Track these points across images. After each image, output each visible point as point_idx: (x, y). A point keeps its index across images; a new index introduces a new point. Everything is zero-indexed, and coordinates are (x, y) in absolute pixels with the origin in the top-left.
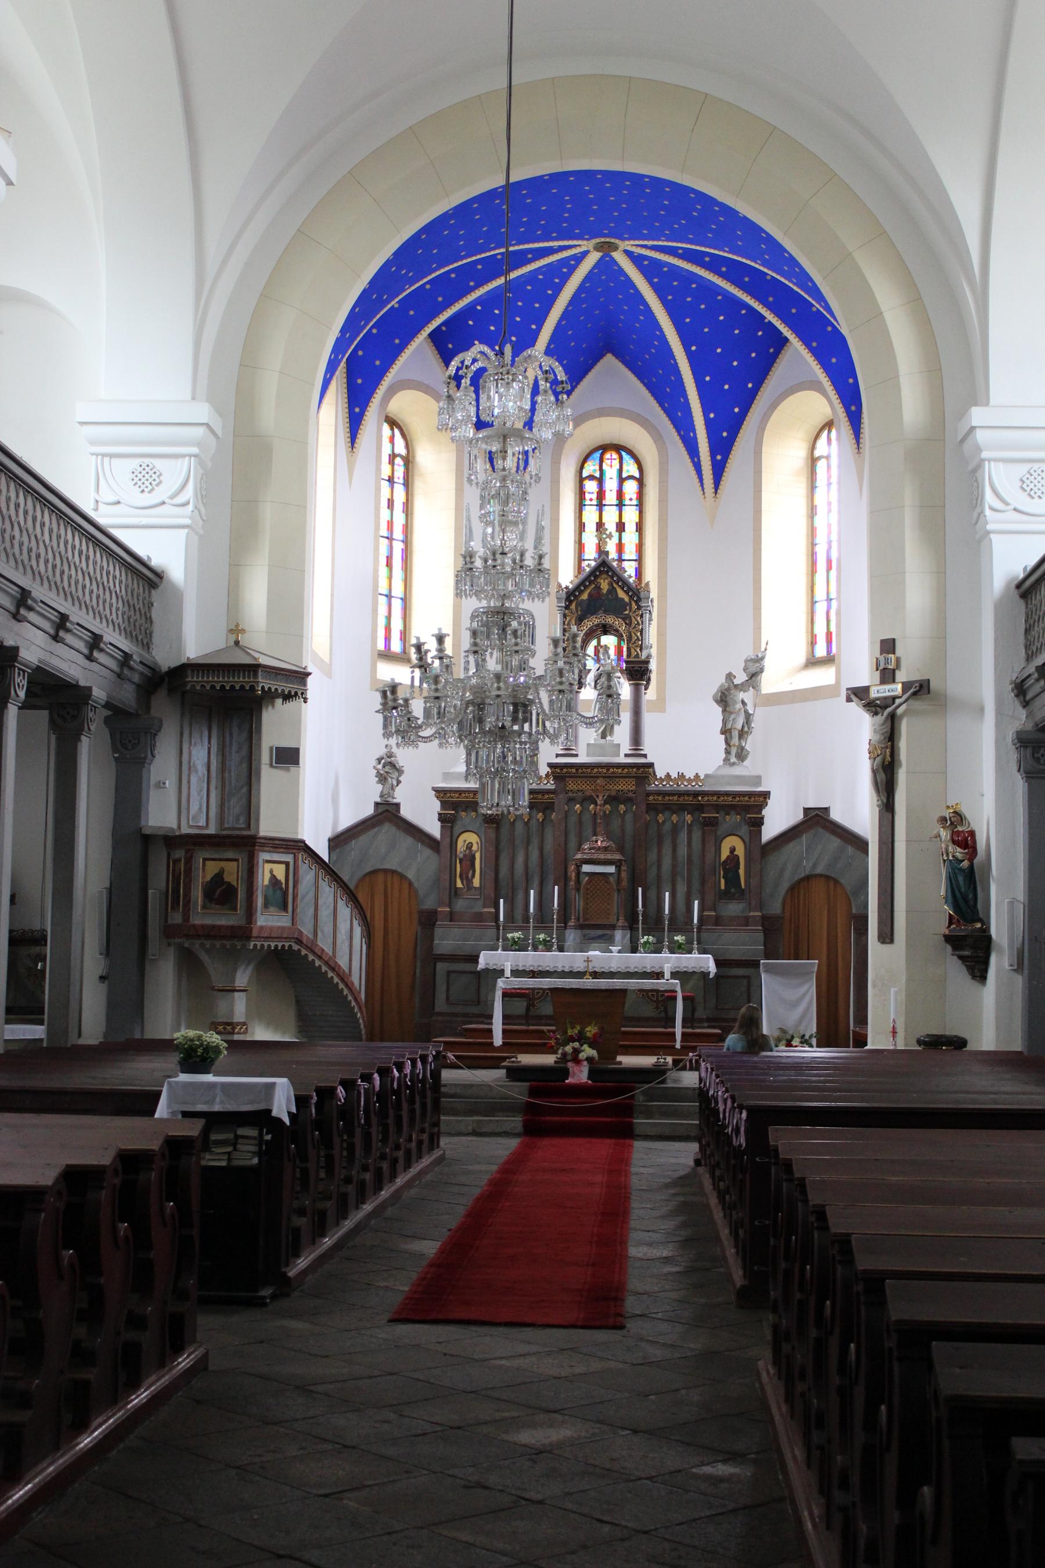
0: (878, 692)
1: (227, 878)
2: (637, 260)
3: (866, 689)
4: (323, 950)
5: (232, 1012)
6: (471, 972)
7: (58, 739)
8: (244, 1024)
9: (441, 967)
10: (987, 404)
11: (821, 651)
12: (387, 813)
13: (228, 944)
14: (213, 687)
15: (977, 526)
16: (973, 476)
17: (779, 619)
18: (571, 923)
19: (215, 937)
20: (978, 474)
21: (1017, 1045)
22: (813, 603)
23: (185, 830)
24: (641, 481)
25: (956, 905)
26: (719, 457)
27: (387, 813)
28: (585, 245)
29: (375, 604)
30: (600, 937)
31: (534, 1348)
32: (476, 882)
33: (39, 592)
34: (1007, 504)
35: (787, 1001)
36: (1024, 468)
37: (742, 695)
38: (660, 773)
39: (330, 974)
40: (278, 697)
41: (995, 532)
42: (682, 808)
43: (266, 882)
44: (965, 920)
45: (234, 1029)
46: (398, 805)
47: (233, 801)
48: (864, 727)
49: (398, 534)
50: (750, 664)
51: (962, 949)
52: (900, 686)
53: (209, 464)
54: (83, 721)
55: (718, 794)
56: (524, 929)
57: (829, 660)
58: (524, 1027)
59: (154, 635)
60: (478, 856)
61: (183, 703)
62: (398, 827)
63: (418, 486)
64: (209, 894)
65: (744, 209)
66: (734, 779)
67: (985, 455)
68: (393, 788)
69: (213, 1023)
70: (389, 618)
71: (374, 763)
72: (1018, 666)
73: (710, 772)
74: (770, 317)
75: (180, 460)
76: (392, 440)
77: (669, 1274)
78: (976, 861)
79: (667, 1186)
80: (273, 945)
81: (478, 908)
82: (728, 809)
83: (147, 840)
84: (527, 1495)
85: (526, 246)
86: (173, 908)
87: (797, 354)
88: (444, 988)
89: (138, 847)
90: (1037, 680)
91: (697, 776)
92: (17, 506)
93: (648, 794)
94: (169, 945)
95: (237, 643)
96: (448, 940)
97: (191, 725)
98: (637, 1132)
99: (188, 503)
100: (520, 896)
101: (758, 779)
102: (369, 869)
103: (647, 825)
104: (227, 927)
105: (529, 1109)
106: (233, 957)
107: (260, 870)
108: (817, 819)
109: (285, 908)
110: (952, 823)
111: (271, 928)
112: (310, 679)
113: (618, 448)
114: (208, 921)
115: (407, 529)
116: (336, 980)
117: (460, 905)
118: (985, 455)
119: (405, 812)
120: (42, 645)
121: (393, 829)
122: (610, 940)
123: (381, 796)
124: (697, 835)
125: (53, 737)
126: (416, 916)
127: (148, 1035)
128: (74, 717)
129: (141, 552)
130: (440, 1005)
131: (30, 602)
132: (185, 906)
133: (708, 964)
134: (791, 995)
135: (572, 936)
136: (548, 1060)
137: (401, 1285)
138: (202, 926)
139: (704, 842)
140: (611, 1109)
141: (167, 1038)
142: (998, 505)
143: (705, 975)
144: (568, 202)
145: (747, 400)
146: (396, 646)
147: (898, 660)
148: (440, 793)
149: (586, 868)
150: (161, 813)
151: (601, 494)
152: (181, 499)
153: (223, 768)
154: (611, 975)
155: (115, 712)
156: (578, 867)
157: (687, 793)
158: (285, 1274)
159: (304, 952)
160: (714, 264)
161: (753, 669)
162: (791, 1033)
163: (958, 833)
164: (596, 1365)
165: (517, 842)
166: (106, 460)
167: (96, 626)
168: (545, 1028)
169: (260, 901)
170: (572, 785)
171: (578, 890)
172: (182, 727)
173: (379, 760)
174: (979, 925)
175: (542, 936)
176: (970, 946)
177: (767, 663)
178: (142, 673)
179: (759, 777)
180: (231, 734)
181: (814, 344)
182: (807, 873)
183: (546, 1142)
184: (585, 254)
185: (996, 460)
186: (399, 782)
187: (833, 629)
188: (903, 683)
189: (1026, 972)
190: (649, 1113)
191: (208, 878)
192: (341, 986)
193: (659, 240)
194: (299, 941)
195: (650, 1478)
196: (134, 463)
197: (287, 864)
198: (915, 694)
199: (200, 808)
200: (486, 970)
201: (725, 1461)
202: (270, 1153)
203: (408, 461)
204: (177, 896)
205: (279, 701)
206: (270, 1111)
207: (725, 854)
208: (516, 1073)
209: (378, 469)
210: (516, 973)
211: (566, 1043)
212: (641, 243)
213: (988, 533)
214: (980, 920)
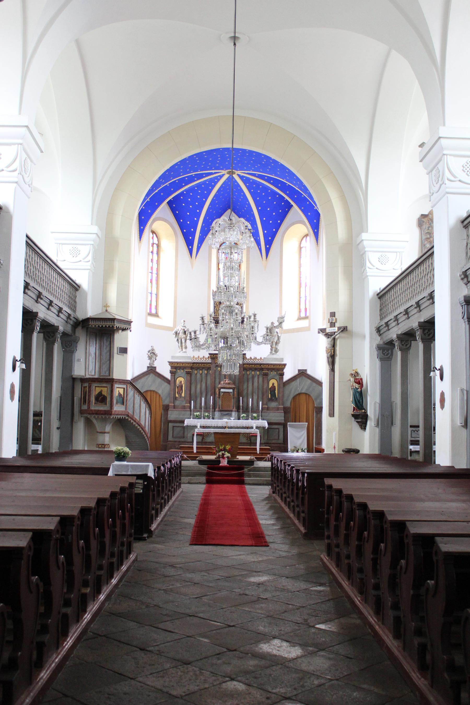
0: (329, 330)
1: (103, 393)
2: (241, 177)
3: (325, 329)
5: (104, 439)
6: (181, 427)
7: (47, 344)
8: (108, 445)
10: (367, 232)
11: (303, 315)
12: (152, 370)
13: (104, 416)
14: (99, 326)
15: (364, 274)
16: (362, 256)
17: (297, 305)
18: (217, 409)
19: (99, 414)
21: (377, 452)
22: (300, 298)
23: (88, 376)
25: (356, 404)
26: (268, 246)
27: (152, 370)
28: (223, 172)
30: (227, 414)
31: (242, 553)
33: (45, 293)
34: (374, 266)
35: (297, 436)
36: (379, 254)
37: (277, 330)
40: (120, 329)
41: (370, 276)
42: (256, 369)
43: (117, 395)
45: (105, 446)
46: (155, 367)
47: (104, 366)
49: (155, 271)
50: (279, 319)
51: (358, 419)
52: (336, 329)
55: (268, 364)
56: (200, 411)
57: (306, 318)
60: (184, 386)
61: (87, 332)
62: (156, 375)
63: (162, 254)
64: (97, 399)
65: (273, 157)
66: (274, 359)
67: (366, 249)
69: (97, 444)
70: (151, 301)
71: (147, 352)
72: (377, 322)
73: (266, 357)
74: (287, 198)
75: (13, 146)
76: (153, 238)
77: (275, 529)
78: (363, 389)
79: (263, 500)
80: (119, 417)
81: (184, 404)
82: (272, 370)
83: (74, 379)
84: (261, 597)
85: (204, 172)
86: (83, 404)
87: (296, 211)
88: (172, 432)
89: (71, 382)
90: (385, 327)
91: (261, 358)
92: (37, 263)
95: (107, 311)
96: (173, 415)
98: (246, 482)
99: (89, 261)
101: (282, 359)
103: (244, 375)
105: (208, 475)
106: (105, 421)
108: (302, 373)
109: (123, 404)
111: (119, 411)
112: (132, 324)
115: (158, 270)
116: (140, 429)
117: (177, 403)
118: (366, 249)
119: (158, 370)
120: (44, 311)
122: (230, 415)
123: (150, 364)
124: (261, 379)
125: (45, 344)
126: (162, 407)
127: (74, 448)
128: (53, 337)
129: (74, 278)
130: (170, 438)
131: (42, 296)
132: (88, 404)
133: (265, 424)
134: (298, 435)
135: (217, 414)
136: (213, 457)
137: (188, 534)
138: (95, 410)
140: (236, 474)
141: (81, 449)
143: (264, 428)
144: (219, 157)
145: (278, 227)
146: (154, 311)
147: (336, 319)
148: (170, 363)
149: (222, 390)
150: (79, 370)
152: (12, 168)
153: (100, 354)
155: (64, 334)
156: (219, 390)
157: (258, 364)
158: (151, 529)
160: (269, 180)
161: (281, 321)
162: (298, 448)
163: (357, 379)
164: (265, 558)
165: (198, 381)
167: (61, 305)
168: (212, 446)
169: (115, 401)
171: (219, 398)
172: (86, 340)
173: (149, 352)
174: (364, 411)
175: (207, 414)
176: (361, 418)
177: (285, 319)
178: (73, 321)
181: (303, 208)
183: (215, 486)
184: (223, 175)
185: (370, 251)
186: (156, 359)
187: (307, 307)
189: (380, 427)
190: (249, 476)
191: (97, 393)
192: (142, 431)
193: (250, 171)
194: (128, 416)
195: (298, 591)
196: (70, 247)
197: (124, 389)
198: (342, 331)
200: (187, 426)
201: (320, 586)
202: (145, 488)
203: (158, 246)
204: (85, 399)
205: (121, 331)
206: (147, 474)
207: (271, 385)
208: (202, 462)
209: (149, 248)
210: (201, 427)
211: (219, 452)
212: (244, 172)
213: (367, 276)
214: (364, 409)
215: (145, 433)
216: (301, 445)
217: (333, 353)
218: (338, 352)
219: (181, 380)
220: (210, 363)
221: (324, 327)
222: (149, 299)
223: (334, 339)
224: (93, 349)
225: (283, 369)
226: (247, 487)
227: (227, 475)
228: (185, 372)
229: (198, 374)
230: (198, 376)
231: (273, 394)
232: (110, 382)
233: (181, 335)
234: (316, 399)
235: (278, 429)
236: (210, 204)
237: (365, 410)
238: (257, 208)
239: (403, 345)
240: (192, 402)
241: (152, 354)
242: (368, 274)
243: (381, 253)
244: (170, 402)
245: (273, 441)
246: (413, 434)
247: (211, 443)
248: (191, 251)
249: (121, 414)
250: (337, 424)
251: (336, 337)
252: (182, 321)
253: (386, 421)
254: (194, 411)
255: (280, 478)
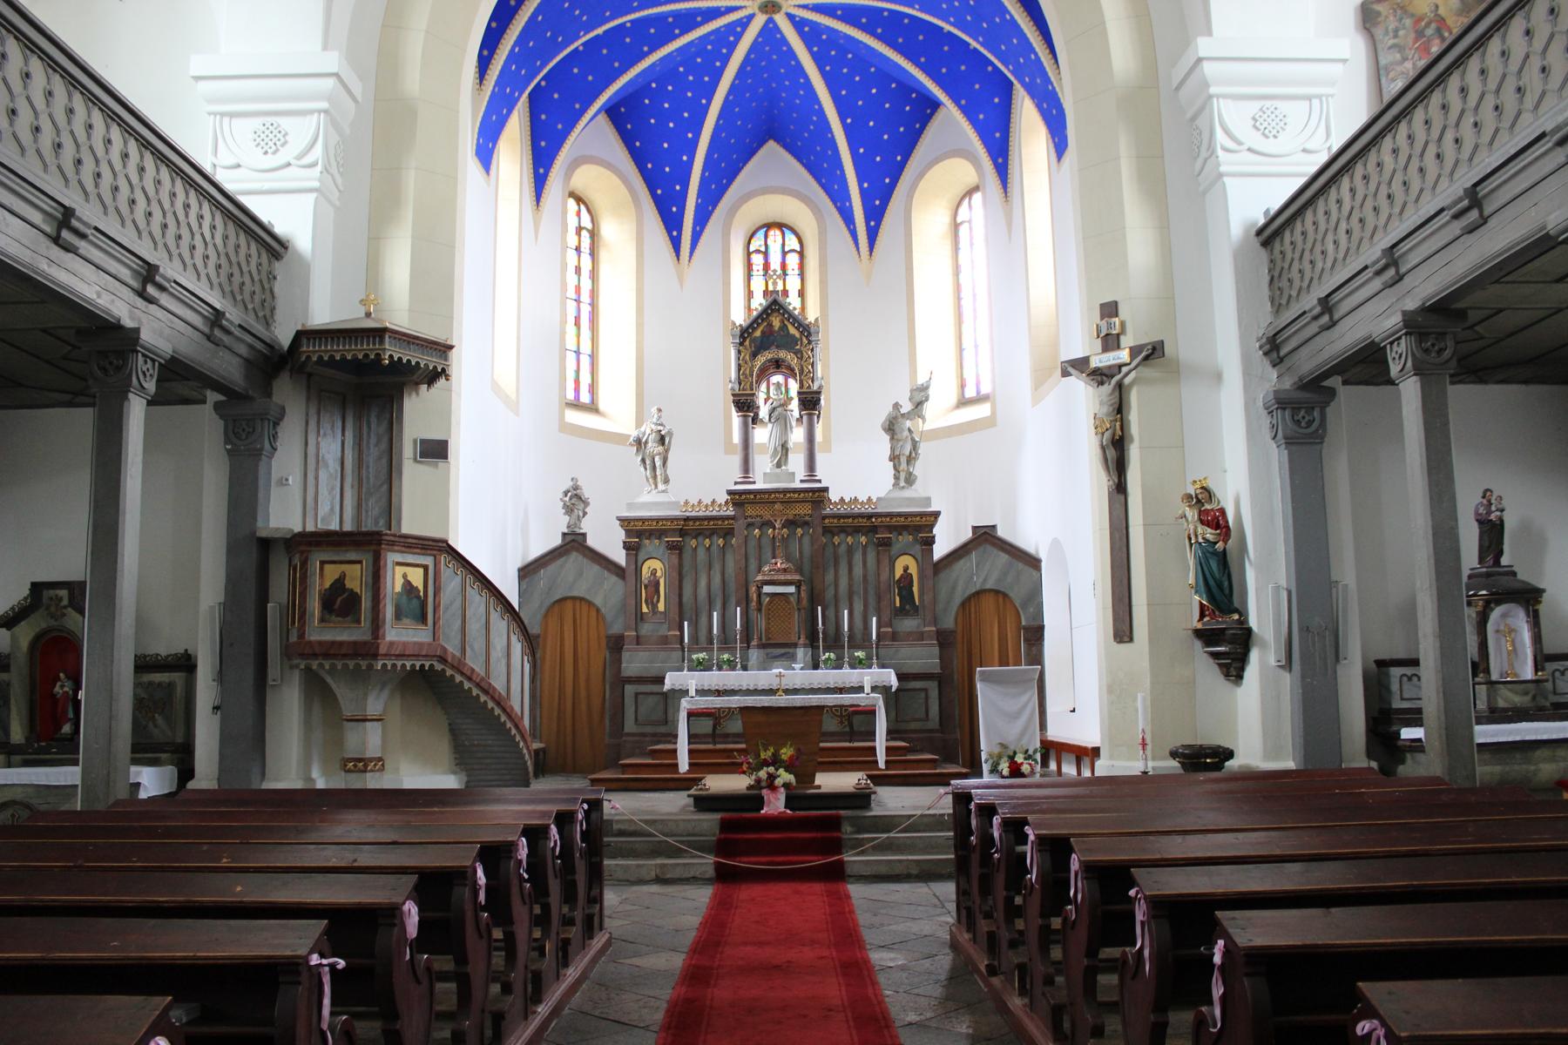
0: (1100, 360)
1: (349, 584)
3: (1086, 360)
4: (473, 670)
8: (380, 759)
9: (630, 689)
12: (574, 542)
13: (351, 664)
18: (754, 643)
19: (335, 656)
20: (1201, 122)
22: (961, 350)
24: (801, 254)
27: (574, 542)
29: (563, 359)
30: (782, 655)
32: (661, 607)
34: (1240, 143)
37: (908, 423)
38: (834, 496)
39: (483, 698)
42: (857, 530)
43: (398, 588)
44: (1221, 611)
45: (366, 766)
46: (584, 535)
47: (372, 501)
48: (1083, 401)
49: (585, 297)
52: (1124, 355)
53: (348, 131)
54: (130, 375)
55: (891, 515)
56: (709, 650)
58: (710, 746)
59: (277, 311)
60: (662, 582)
61: (309, 387)
63: (603, 255)
64: (328, 603)
66: (905, 502)
67: (1213, 90)
68: (579, 519)
71: (561, 495)
72: (1264, 320)
73: (882, 495)
75: (308, 118)
81: (663, 630)
82: (900, 529)
83: (266, 545)
89: (260, 557)
91: (869, 499)
93: (824, 518)
94: (292, 667)
96: (634, 663)
97: (319, 414)
98: (849, 871)
99: (314, 164)
100: (703, 620)
102: (557, 597)
103: (824, 547)
104: (349, 643)
105: (722, 847)
106: (362, 678)
107: (389, 574)
108: (985, 537)
110: (1199, 501)
111: (405, 644)
112: (454, 354)
113: (781, 226)
114: (328, 636)
115: (594, 294)
116: (491, 704)
117: (646, 629)
118: (1213, 90)
119: (591, 542)
121: (580, 557)
122: (793, 658)
124: (871, 556)
128: (118, 369)
129: (264, 218)
130: (630, 726)
134: (1011, 705)
135: (754, 655)
138: (321, 643)
139: (878, 561)
142: (1230, 144)
145: (897, 171)
146: (585, 398)
147: (1123, 324)
148: (624, 522)
149: (767, 589)
150: (284, 514)
151: (766, 266)
152: (308, 159)
153: (360, 463)
154: (795, 691)
156: (759, 588)
159: (449, 672)
161: (918, 398)
162: (1012, 748)
163: (1207, 511)
166: (226, 120)
169: (389, 611)
170: (750, 511)
171: (759, 610)
173: (566, 494)
174: (1236, 617)
175: (726, 656)
176: (1227, 643)
177: (931, 392)
178: (251, 346)
179: (929, 499)
180: (369, 427)
182: (978, 587)
184: (751, 17)
185: (1225, 96)
186: (585, 514)
188: (1131, 349)
191: (327, 585)
192: (497, 711)
194: (443, 660)
196: (256, 123)
197: (426, 568)
198: (1147, 358)
199: (332, 509)
200: (673, 691)
203: (593, 234)
204: (296, 612)
207: (899, 573)
208: (706, 803)
210: (701, 692)
214: (1237, 611)
215: (509, 716)
216: (1022, 734)
217: (1119, 432)
218: (1134, 429)
219: (654, 567)
220: (733, 518)
221: (1080, 355)
222: (570, 376)
223: (1120, 385)
224: (332, 445)
225: (932, 526)
226: (856, 891)
227: (783, 845)
228: (664, 545)
229: (699, 548)
230: (701, 553)
231: (907, 595)
232: (369, 543)
233: (653, 447)
234: (1025, 605)
235: (926, 690)
236: (720, 117)
237: (1240, 615)
238: (843, 121)
239: (1426, 351)
240: (687, 633)
241: (575, 501)
242: (1222, 169)
243: (1262, 103)
244: (627, 628)
245: (913, 726)
246: (1405, 687)
247: (737, 737)
248: (676, 244)
249: (417, 656)
250: (1145, 664)
251: (1127, 381)
252: (654, 410)
253: (1315, 644)
254: (691, 651)
255: (991, 865)
